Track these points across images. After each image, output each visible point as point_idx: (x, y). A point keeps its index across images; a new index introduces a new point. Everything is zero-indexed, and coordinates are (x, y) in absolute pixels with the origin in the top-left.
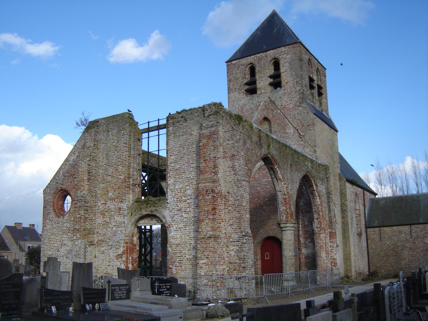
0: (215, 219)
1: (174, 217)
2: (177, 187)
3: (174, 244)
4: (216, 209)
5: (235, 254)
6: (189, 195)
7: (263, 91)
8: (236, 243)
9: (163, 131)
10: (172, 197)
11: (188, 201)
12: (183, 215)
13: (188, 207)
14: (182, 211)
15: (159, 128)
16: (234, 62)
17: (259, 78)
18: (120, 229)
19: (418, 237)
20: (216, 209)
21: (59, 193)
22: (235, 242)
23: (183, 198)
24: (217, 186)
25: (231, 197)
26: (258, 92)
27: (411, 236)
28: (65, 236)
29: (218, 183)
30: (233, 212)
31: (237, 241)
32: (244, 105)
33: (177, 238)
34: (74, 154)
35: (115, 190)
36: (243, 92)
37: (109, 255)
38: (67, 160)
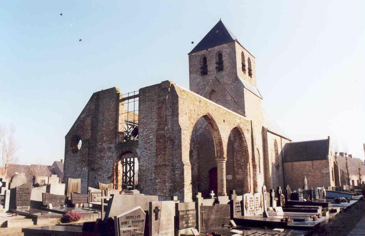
0: (166, 154)
1: (142, 153)
2: (144, 134)
3: (142, 170)
4: (166, 147)
5: (179, 176)
6: (151, 139)
7: (211, 73)
8: (179, 169)
9: (137, 99)
10: (141, 140)
11: (151, 143)
12: (148, 152)
13: (151, 147)
14: (147, 149)
15: (134, 97)
16: (193, 54)
17: (209, 64)
18: (110, 160)
19: (316, 169)
20: (166, 147)
21: (74, 139)
22: (178, 168)
23: (148, 141)
24: (167, 133)
25: (177, 140)
26: (209, 73)
27: (313, 167)
28: (77, 165)
29: (169, 131)
30: (177, 150)
31: (180, 168)
32: (199, 82)
33: (144, 166)
34: (84, 114)
35: (107, 136)
36: (199, 74)
37: (104, 177)
38: (79, 117)
